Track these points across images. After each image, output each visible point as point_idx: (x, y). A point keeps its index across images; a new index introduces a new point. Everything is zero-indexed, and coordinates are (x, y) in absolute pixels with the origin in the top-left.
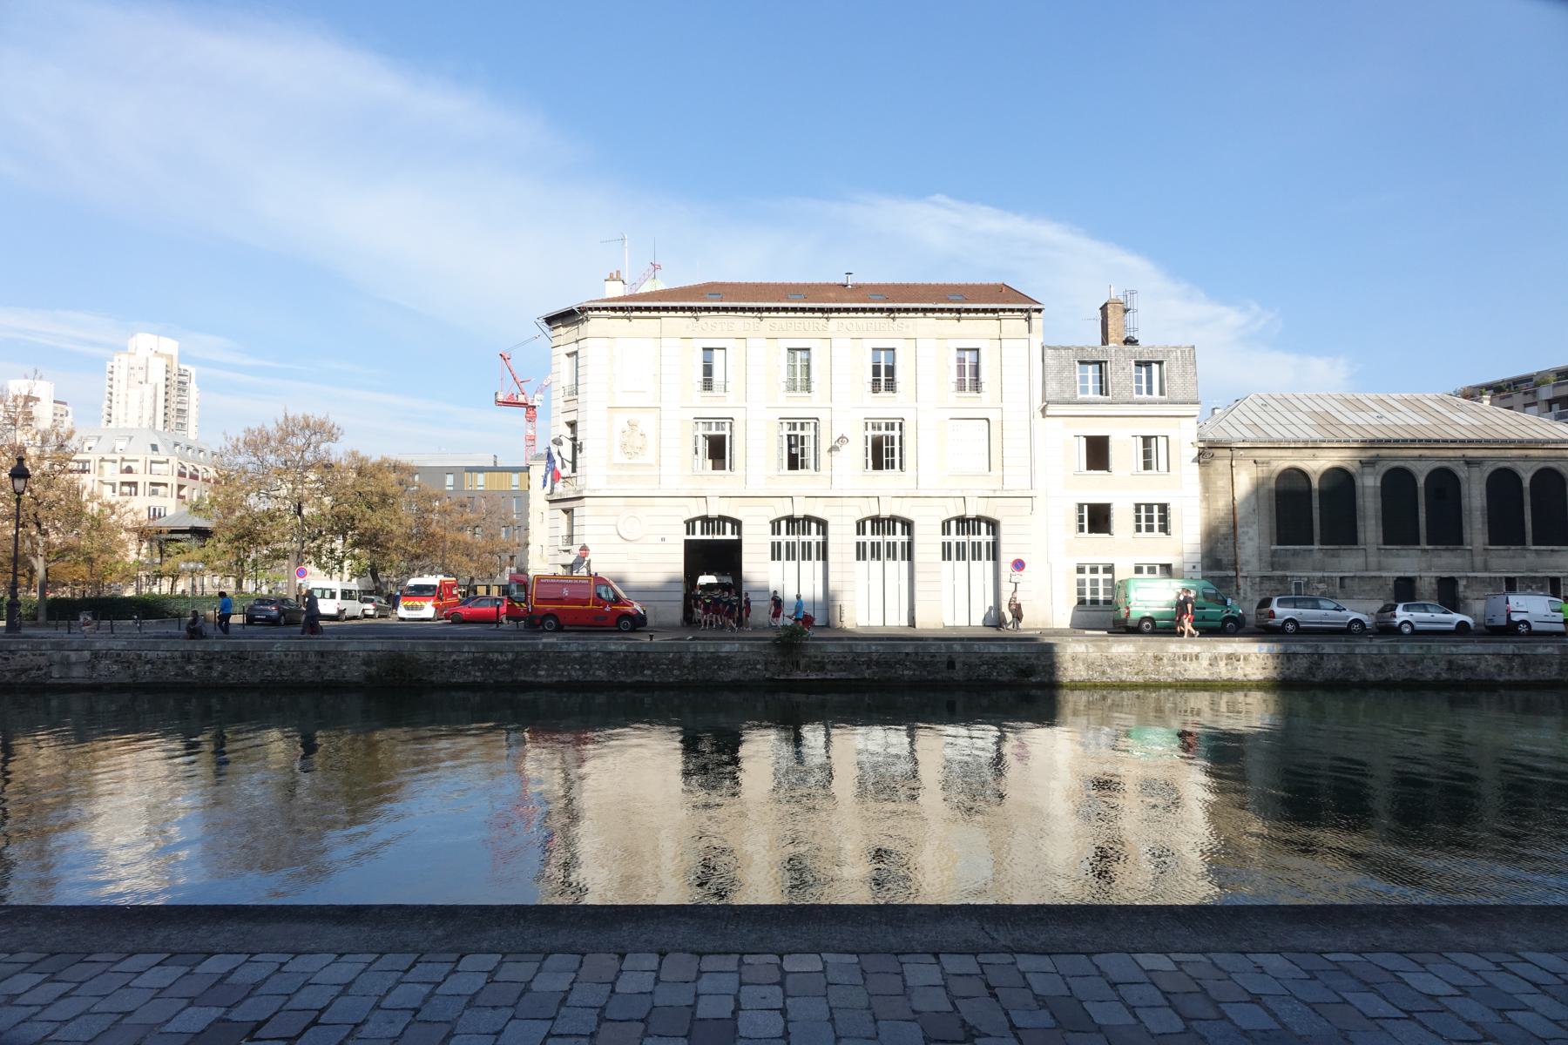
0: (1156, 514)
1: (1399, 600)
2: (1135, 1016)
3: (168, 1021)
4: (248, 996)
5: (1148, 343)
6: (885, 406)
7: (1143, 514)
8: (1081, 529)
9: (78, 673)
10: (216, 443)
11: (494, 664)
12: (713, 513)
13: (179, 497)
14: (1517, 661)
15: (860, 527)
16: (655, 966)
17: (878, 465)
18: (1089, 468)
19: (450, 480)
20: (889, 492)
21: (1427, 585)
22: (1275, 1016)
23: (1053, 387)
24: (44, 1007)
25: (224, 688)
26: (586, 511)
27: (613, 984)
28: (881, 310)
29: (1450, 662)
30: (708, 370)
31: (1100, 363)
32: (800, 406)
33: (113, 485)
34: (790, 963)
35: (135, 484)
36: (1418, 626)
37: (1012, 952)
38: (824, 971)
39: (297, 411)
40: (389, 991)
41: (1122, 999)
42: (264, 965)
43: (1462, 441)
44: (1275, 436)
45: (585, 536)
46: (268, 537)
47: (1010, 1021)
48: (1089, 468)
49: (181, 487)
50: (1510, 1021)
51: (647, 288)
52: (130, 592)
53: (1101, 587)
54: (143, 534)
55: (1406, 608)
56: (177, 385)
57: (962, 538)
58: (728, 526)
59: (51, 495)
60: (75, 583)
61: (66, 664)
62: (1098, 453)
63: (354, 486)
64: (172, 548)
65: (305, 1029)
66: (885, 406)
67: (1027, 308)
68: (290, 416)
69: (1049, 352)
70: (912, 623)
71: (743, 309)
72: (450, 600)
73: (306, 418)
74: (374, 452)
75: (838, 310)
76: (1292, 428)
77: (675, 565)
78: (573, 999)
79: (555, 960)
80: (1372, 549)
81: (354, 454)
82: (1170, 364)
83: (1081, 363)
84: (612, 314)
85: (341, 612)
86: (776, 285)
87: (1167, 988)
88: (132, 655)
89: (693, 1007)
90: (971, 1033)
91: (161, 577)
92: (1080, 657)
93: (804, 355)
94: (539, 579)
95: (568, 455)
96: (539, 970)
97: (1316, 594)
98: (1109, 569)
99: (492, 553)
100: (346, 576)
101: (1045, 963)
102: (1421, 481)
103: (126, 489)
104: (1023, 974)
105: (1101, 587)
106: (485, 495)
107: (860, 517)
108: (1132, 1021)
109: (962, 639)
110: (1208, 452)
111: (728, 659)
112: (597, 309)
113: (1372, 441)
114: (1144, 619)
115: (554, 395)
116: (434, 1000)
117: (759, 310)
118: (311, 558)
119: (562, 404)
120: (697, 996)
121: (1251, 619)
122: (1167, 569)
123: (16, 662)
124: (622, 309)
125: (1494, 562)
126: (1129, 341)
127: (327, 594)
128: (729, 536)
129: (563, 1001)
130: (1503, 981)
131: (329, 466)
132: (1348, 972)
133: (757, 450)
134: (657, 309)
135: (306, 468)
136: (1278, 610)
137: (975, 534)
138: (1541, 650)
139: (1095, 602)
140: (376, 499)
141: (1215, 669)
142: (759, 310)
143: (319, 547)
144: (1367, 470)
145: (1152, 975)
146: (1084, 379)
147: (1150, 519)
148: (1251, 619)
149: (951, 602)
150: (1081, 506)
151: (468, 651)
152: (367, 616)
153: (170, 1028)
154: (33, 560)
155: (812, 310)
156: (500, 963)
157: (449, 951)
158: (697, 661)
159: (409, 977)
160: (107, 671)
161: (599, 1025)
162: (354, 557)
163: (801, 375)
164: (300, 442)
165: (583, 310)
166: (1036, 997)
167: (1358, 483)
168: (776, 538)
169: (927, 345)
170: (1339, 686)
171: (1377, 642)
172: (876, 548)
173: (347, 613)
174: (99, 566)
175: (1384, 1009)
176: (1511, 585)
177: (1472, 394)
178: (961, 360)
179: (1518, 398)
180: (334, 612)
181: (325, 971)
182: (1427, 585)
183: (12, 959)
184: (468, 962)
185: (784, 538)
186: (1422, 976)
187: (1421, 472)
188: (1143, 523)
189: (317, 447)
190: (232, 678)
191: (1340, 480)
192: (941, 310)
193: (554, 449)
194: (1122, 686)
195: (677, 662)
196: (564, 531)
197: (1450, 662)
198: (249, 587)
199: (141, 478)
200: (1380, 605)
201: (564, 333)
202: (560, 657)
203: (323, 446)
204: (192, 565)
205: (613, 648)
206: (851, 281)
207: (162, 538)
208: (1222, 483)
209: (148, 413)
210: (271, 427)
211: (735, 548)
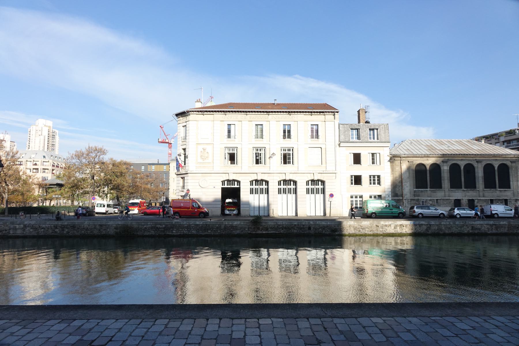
0: (376, 179)
1: (456, 207)
2: (371, 336)
3: (63, 340)
4: (88, 332)
5: (374, 122)
6: (287, 143)
7: (372, 179)
8: (352, 184)
9: (19, 232)
10: (66, 155)
12: (231, 178)
13: (52, 173)
14: (494, 226)
15: (279, 183)
16: (218, 323)
17: (285, 163)
18: (354, 164)
19: (143, 168)
20: (288, 171)
21: (464, 202)
22: (414, 336)
23: (342, 137)
24: (23, 336)
25: (68, 237)
26: (189, 178)
27: (205, 328)
28: (286, 112)
29: (472, 227)
30: (229, 132)
31: (357, 129)
32: (259, 143)
33: (30, 169)
34: (261, 321)
35: (38, 169)
36: (462, 215)
37: (332, 318)
38: (272, 324)
39: (93, 145)
40: (134, 330)
41: (366, 331)
42: (93, 323)
43: (475, 155)
44: (415, 153)
45: (189, 186)
46: (82, 187)
47: (332, 338)
48: (354, 164)
49: (53, 170)
50: (488, 337)
51: (209, 104)
52: (35, 205)
53: (358, 203)
54: (40, 186)
55: (458, 209)
56: (52, 136)
57: (313, 187)
58: (236, 183)
59: (10, 172)
60: (17, 202)
61: (15, 229)
62: (357, 159)
63: (111, 170)
64: (50, 190)
65: (108, 342)
66: (287, 143)
67: (334, 111)
68: (90, 146)
69: (341, 126)
70: (325, 214)
71: (241, 112)
72: (143, 208)
73: (96, 147)
74: (118, 159)
75: (272, 112)
76: (420, 150)
77: (218, 195)
78: (193, 332)
79: (186, 321)
80: (447, 190)
81: (111, 159)
82: (380, 130)
83: (351, 129)
84: (198, 113)
85: (107, 211)
86: (251, 104)
87: (381, 328)
88: (37, 226)
89: (231, 335)
90: (319, 342)
91: (46, 200)
92: (350, 226)
93: (261, 127)
94: (173, 200)
95: (183, 159)
96: (181, 324)
97: (429, 205)
98: (361, 197)
99: (157, 192)
100: (108, 200)
101: (342, 321)
102: (462, 168)
103: (35, 171)
104: (336, 324)
105: (358, 203)
106: (155, 173)
107: (279, 180)
108: (370, 338)
109: (313, 220)
110: (393, 158)
111: (236, 227)
112: (193, 111)
113: (443, 155)
114: (373, 213)
115: (178, 140)
116: (148, 333)
117: (246, 112)
118: (96, 193)
119: (181, 143)
120: (232, 331)
121: (408, 213)
122: (380, 197)
124: (201, 111)
125: (486, 194)
126: (367, 122)
127: (102, 206)
128: (236, 186)
129: (190, 334)
130: (486, 325)
131: (103, 163)
132: (438, 323)
133: (246, 158)
134: (212, 111)
135: (96, 164)
136: (416, 210)
137: (317, 185)
138: (502, 223)
139: (356, 208)
140: (119, 174)
141: (396, 230)
142: (246, 112)
143: (99, 190)
144: (445, 164)
145: (376, 324)
146: (352, 135)
147: (374, 180)
148: (408, 213)
149: (310, 208)
150: (352, 176)
151: (149, 224)
152: (115, 213)
153: (64, 342)
154: (4, 195)
155: (263, 112)
156: (169, 322)
157: (152, 318)
158: (226, 227)
159: (140, 326)
160: (29, 231)
161: (201, 341)
162: (111, 193)
163: (260, 134)
164: (93, 155)
165: (188, 112)
166: (340, 331)
167: (442, 168)
168: (252, 187)
169: (301, 123)
170: (438, 235)
171: (449, 220)
172: (284, 190)
173: (109, 212)
174: (25, 197)
175: (448, 333)
176: (492, 202)
177: (478, 139)
178: (312, 128)
179: (493, 141)
180: (104, 211)
181: (112, 325)
182: (464, 202)
183: (11, 321)
184: (158, 322)
185: (254, 187)
186: (461, 324)
187: (462, 164)
188: (372, 182)
189: (99, 157)
190: (71, 234)
191: (436, 167)
192: (306, 112)
193: (178, 157)
194: (365, 235)
195: (219, 228)
196: (181, 184)
197: (472, 227)
198: (76, 203)
199: (39, 167)
200: (450, 208)
201: (182, 119)
202: (181, 226)
203: (101, 157)
204: (57, 196)
205: (198, 223)
206: (276, 102)
207: (46, 187)
208: (398, 169)
209: (42, 145)
210: (84, 150)
211: (238, 190)
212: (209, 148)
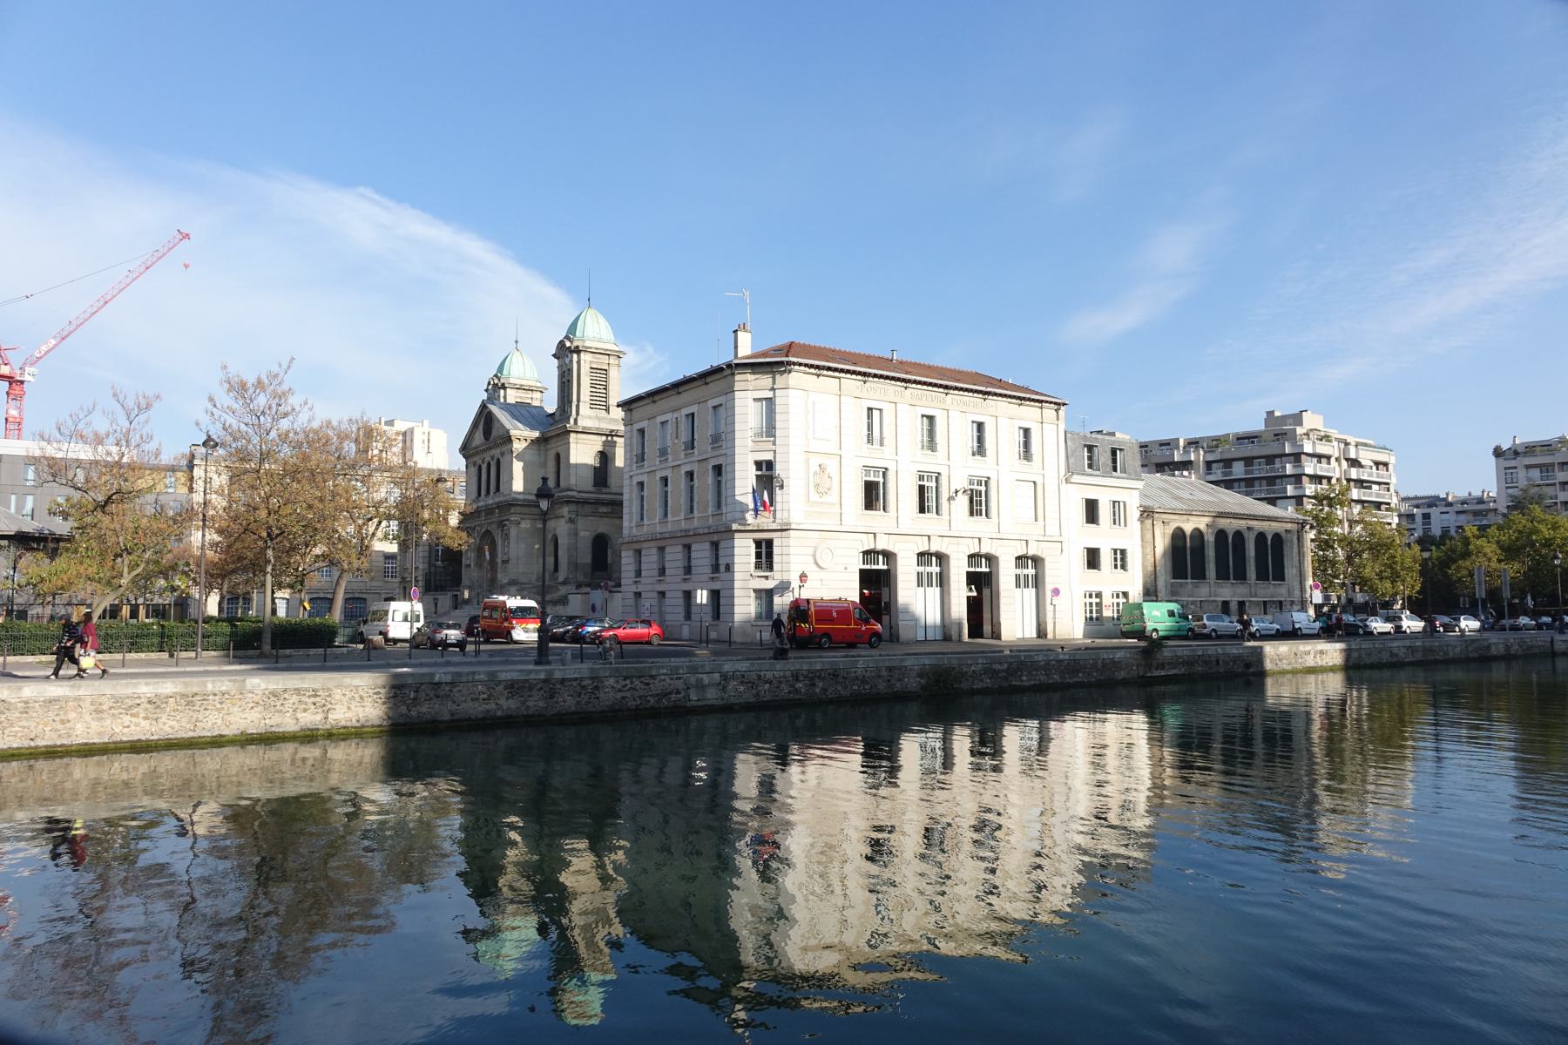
9: (712, 695)
11: (996, 672)
25: (812, 704)
61: (701, 687)
70: (1041, 633)
88: (753, 676)
110: (1147, 513)
123: (657, 686)
128: (881, 566)
190: (831, 693)
212: (832, 466)
